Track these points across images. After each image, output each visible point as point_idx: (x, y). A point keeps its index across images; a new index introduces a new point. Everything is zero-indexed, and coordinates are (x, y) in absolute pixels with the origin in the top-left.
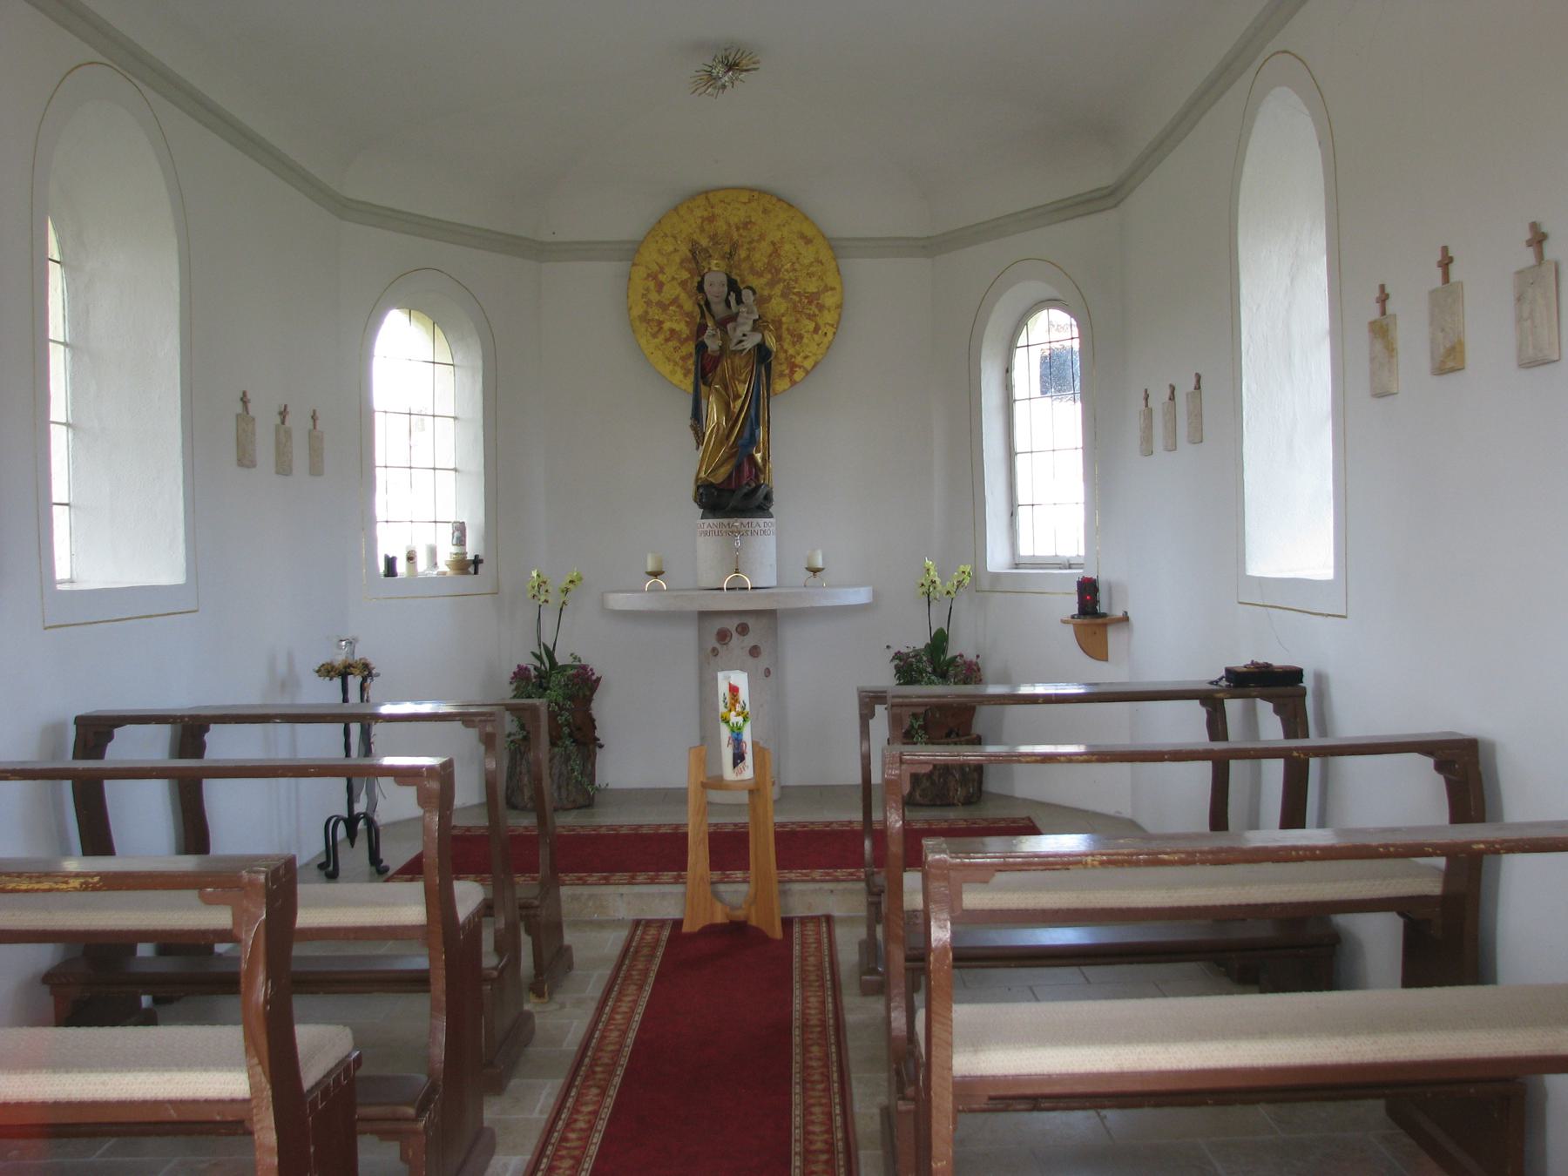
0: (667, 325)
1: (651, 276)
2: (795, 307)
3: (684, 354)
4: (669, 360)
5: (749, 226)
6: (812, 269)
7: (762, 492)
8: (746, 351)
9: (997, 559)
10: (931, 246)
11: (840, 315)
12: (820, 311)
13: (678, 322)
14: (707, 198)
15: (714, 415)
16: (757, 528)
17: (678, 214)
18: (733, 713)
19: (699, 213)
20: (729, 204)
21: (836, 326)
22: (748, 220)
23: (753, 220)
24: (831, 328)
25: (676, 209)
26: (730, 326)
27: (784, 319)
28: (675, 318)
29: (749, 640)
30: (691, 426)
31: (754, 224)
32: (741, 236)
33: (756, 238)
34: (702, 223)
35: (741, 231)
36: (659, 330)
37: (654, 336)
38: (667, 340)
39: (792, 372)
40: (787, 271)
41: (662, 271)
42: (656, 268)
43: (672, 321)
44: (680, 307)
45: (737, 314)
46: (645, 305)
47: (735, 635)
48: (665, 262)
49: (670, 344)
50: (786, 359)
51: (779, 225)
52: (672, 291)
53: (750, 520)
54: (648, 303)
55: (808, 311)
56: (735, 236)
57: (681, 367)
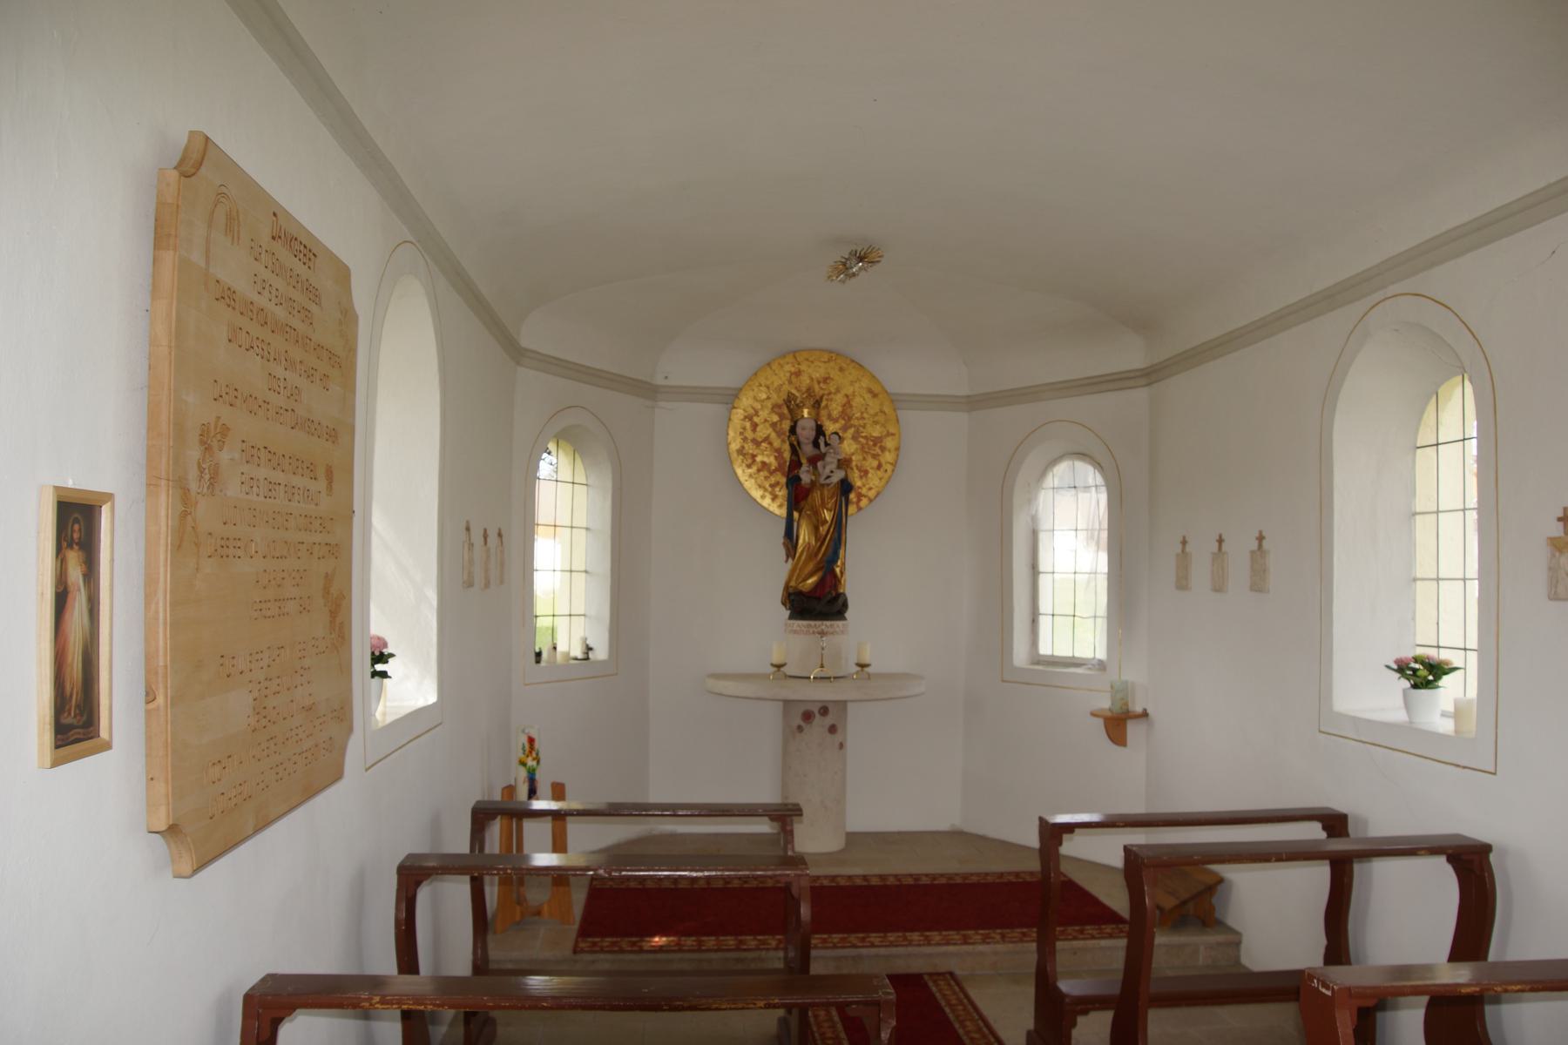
0: (759, 459)
2: (863, 447)
4: (760, 486)
5: (828, 381)
6: (876, 419)
7: (840, 601)
8: (832, 485)
9: (1020, 656)
10: (973, 403)
11: (898, 456)
14: (795, 357)
15: (804, 536)
17: (771, 368)
18: (530, 758)
19: (788, 368)
20: (812, 362)
21: (894, 464)
22: (827, 376)
23: (832, 376)
25: (769, 364)
26: (820, 464)
27: (854, 458)
28: (765, 453)
29: (829, 720)
30: (784, 544)
31: (832, 379)
32: (822, 389)
33: (833, 390)
35: (822, 385)
37: (749, 466)
38: (759, 471)
40: (857, 419)
41: (757, 414)
42: (752, 411)
43: (763, 454)
44: (770, 444)
45: (825, 455)
47: (817, 715)
48: (759, 407)
49: (762, 473)
51: (852, 382)
52: (764, 431)
53: (832, 622)
54: (745, 439)
56: (816, 387)
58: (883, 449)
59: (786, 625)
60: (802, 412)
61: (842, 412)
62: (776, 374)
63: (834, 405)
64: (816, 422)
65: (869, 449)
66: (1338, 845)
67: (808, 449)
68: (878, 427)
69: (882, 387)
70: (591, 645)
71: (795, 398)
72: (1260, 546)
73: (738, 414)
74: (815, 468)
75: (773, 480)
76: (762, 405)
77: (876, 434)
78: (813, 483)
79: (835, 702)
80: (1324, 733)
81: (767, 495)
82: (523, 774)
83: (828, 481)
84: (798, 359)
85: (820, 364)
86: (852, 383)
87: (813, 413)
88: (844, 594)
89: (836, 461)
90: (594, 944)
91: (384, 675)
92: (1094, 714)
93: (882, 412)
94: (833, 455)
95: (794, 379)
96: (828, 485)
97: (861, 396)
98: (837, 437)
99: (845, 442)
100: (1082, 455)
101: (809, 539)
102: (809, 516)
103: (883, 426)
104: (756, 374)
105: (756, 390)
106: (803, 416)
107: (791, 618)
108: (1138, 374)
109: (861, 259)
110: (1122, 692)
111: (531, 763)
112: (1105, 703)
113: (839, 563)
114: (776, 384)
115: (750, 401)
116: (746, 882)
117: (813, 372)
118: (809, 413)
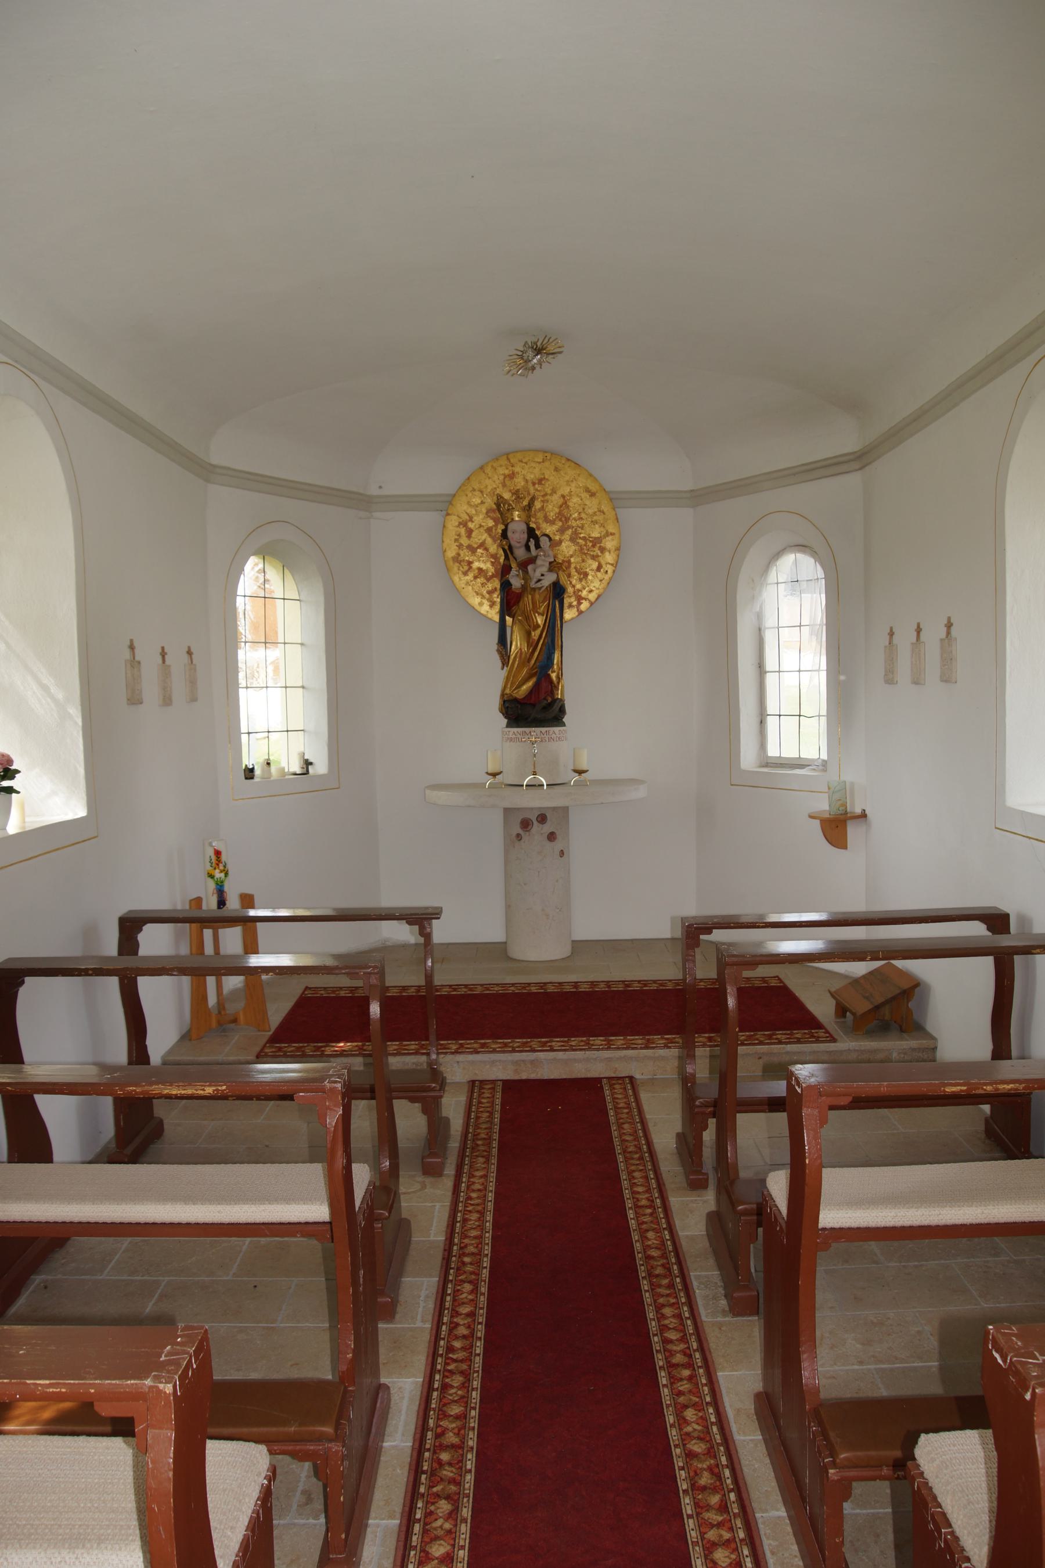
0: (476, 565)
2: (581, 549)
4: (477, 594)
5: (543, 482)
6: (595, 518)
7: (556, 708)
9: (748, 759)
10: (698, 498)
11: (618, 556)
14: (508, 459)
15: (517, 643)
18: (217, 871)
19: (503, 471)
20: (526, 463)
23: (546, 477)
25: (482, 468)
26: (530, 568)
27: (572, 560)
29: (547, 828)
30: (498, 651)
32: (537, 490)
33: (549, 492)
35: (537, 486)
37: (465, 574)
38: (475, 577)
39: (579, 604)
41: (471, 520)
42: (465, 517)
43: (479, 561)
44: (486, 549)
45: (536, 557)
47: (535, 823)
48: (474, 512)
50: (574, 592)
54: (460, 546)
57: (488, 600)
58: (603, 550)
59: (503, 732)
60: (512, 515)
62: (489, 478)
63: (550, 507)
64: (528, 525)
65: (588, 550)
66: (1004, 941)
67: (520, 553)
68: (597, 526)
69: (601, 486)
70: (311, 760)
71: (505, 502)
72: (948, 633)
73: (452, 522)
74: (526, 572)
75: (489, 586)
76: (476, 511)
77: (595, 534)
78: (524, 588)
79: (554, 809)
80: (998, 829)
81: (485, 602)
82: (211, 885)
83: (539, 585)
84: (512, 461)
85: (533, 465)
86: (568, 483)
87: (524, 516)
88: (562, 700)
89: (547, 564)
90: (506, 1045)
91: (10, 790)
94: (543, 557)
95: (508, 483)
96: (540, 588)
97: (578, 495)
98: (547, 539)
99: (563, 544)
100: (802, 547)
101: (521, 644)
103: (602, 526)
104: (469, 478)
105: (470, 495)
106: (513, 519)
107: (508, 726)
108: (851, 457)
109: (538, 351)
110: (840, 792)
111: (218, 875)
112: (823, 805)
114: (490, 488)
115: (465, 507)
116: (645, 985)
117: (527, 473)
118: (519, 516)
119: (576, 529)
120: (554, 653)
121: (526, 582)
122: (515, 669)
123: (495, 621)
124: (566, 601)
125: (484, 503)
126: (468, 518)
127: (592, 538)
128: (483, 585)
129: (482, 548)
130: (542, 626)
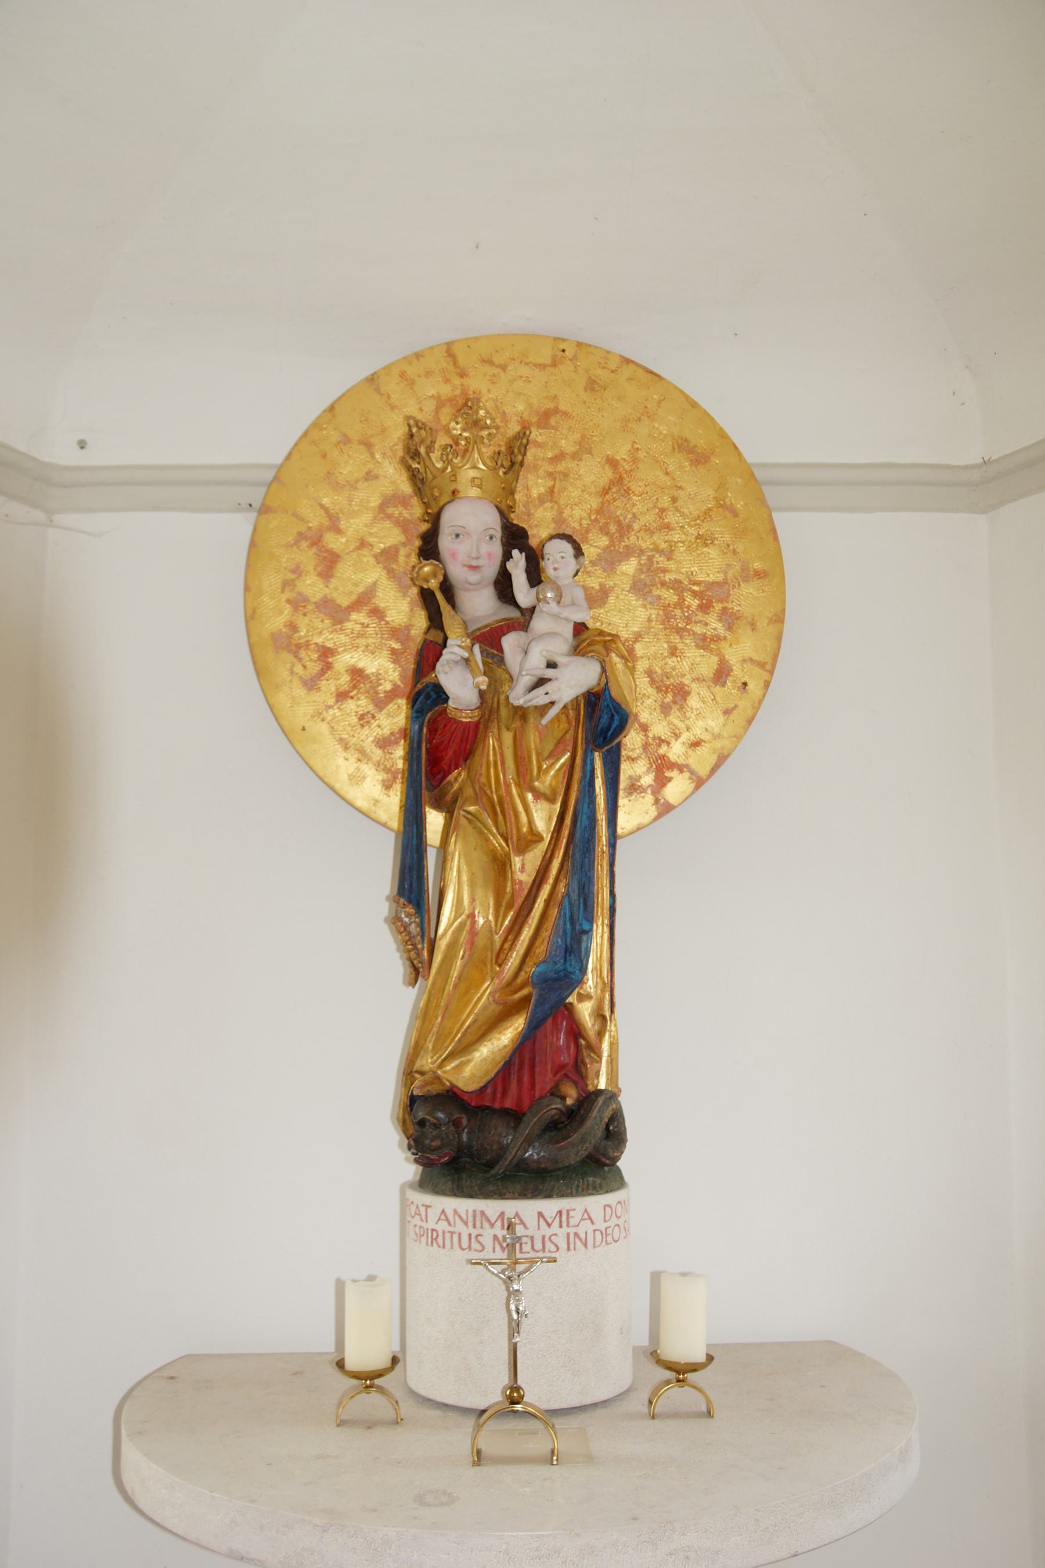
0: (345, 660)
1: (306, 538)
2: (667, 617)
3: (386, 732)
5: (553, 421)
12: (730, 628)
13: (371, 651)
16: (586, 1225)
17: (378, 390)
20: (503, 367)
21: (768, 666)
22: (551, 405)
24: (757, 670)
30: (395, 921)
34: (437, 411)
36: (322, 673)
37: (311, 684)
39: (661, 781)
40: (648, 530)
42: (315, 519)
44: (378, 613)
46: (288, 609)
49: (350, 705)
50: (646, 746)
54: (298, 604)
55: (698, 629)
57: (378, 764)
59: (404, 1203)
61: (600, 511)
63: (574, 493)
68: (712, 552)
81: (368, 770)
85: (524, 371)
92: (556, 679)
93: (722, 505)
96: (543, 709)
101: (473, 900)
102: (472, 818)
113: (591, 982)
119: (650, 559)
120: (588, 932)
121: (495, 683)
122: (450, 987)
123: (384, 825)
124: (626, 770)
125: (377, 477)
126: (326, 522)
127: (698, 583)
128: (364, 719)
129: (366, 609)
130: (547, 837)
